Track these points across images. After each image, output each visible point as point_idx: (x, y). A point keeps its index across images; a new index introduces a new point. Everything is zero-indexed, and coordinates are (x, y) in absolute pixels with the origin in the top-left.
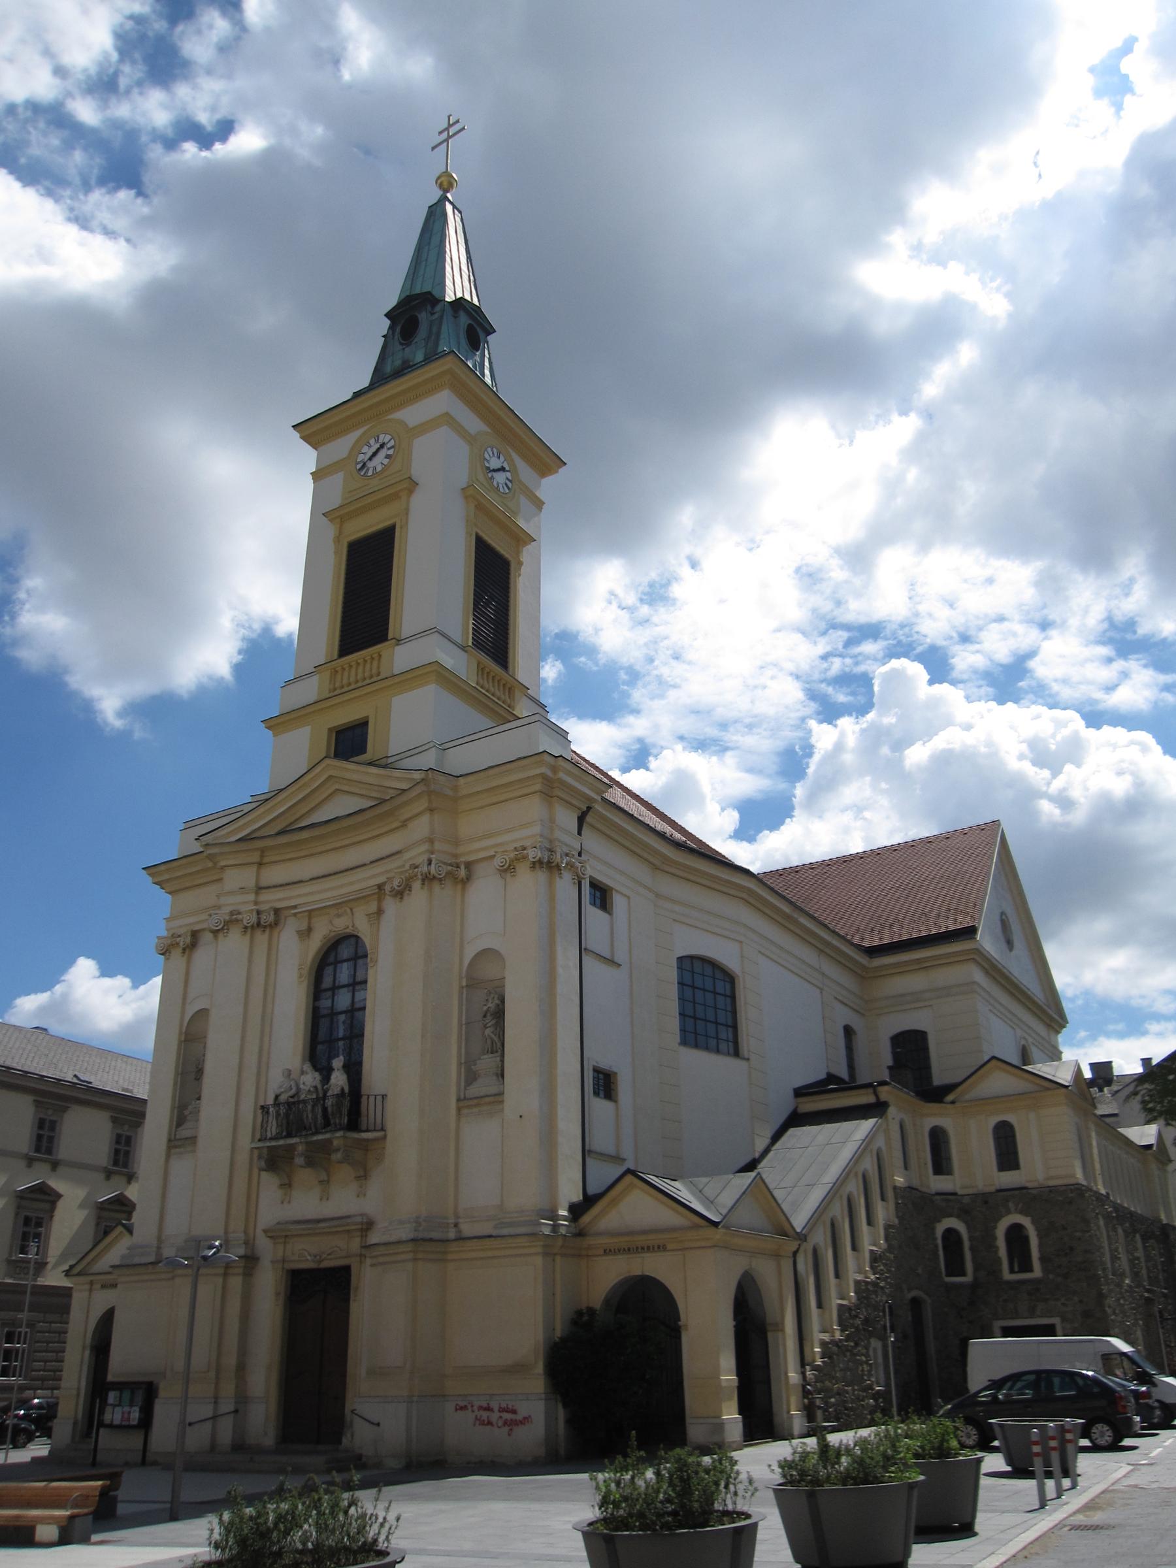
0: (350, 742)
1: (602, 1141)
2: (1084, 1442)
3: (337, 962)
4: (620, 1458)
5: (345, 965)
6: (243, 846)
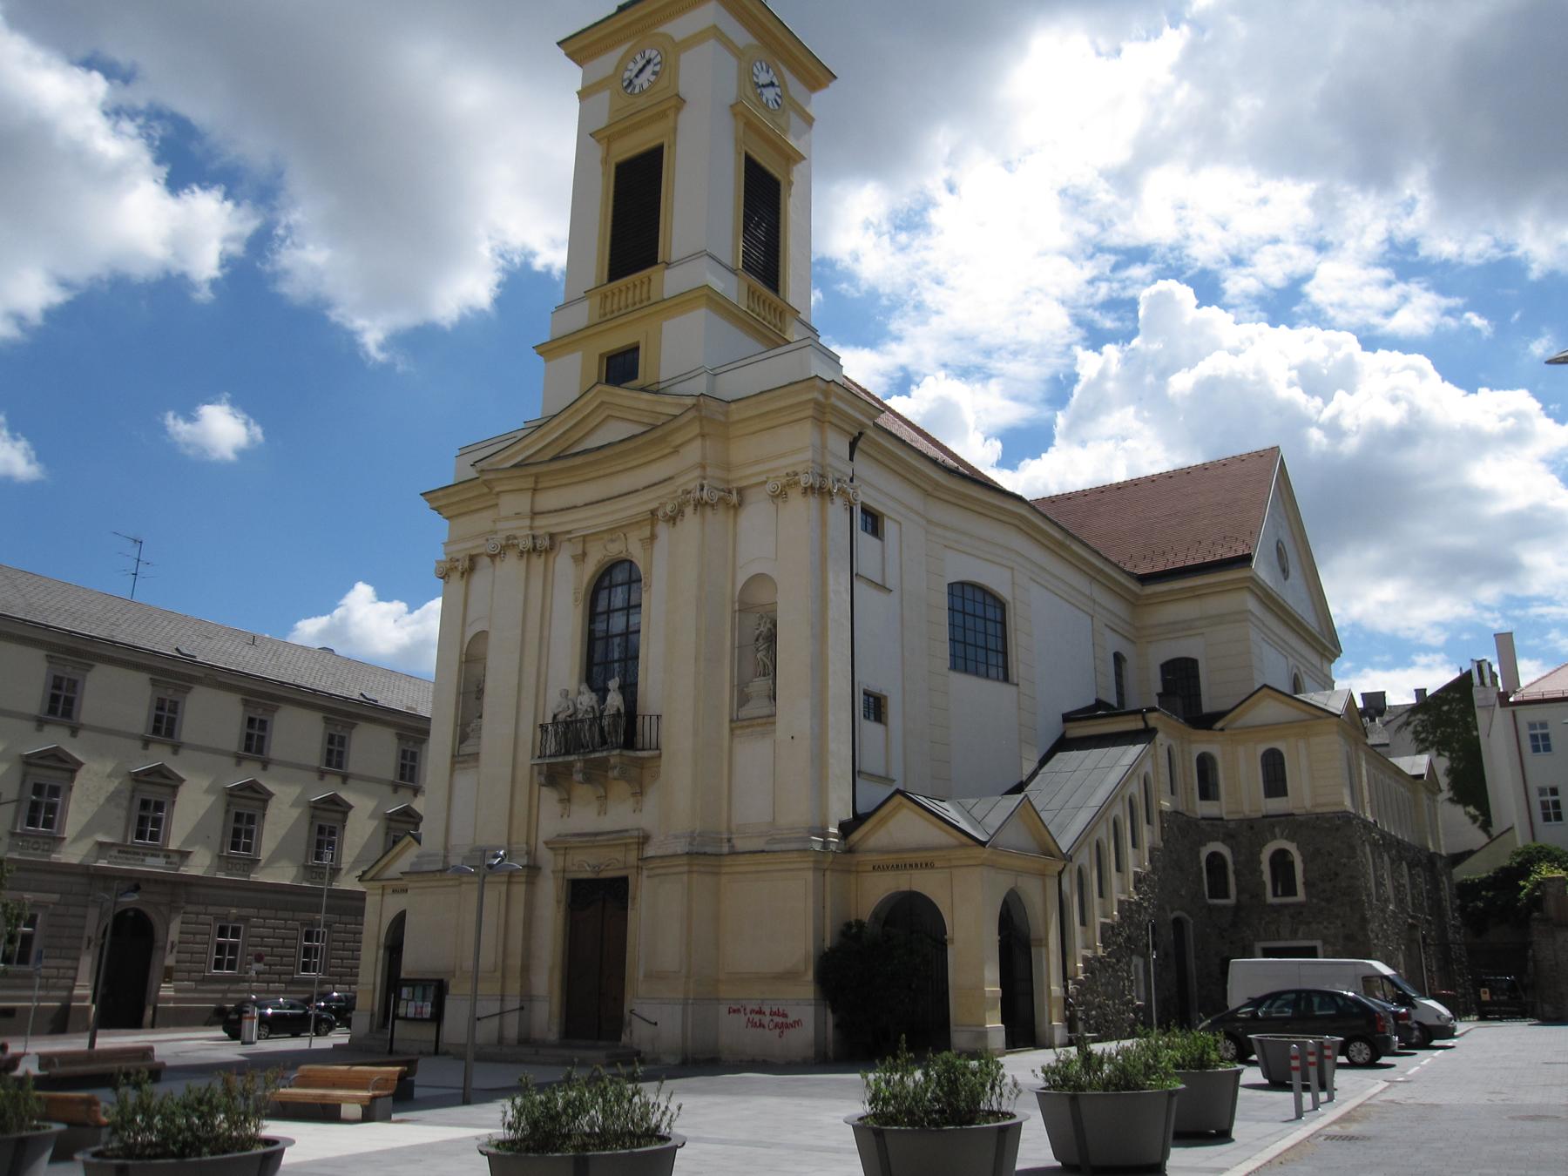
0: (621, 367)
1: (872, 761)
2: (1342, 1059)
3: (611, 587)
4: (890, 1059)
5: (619, 589)
6: (517, 472)
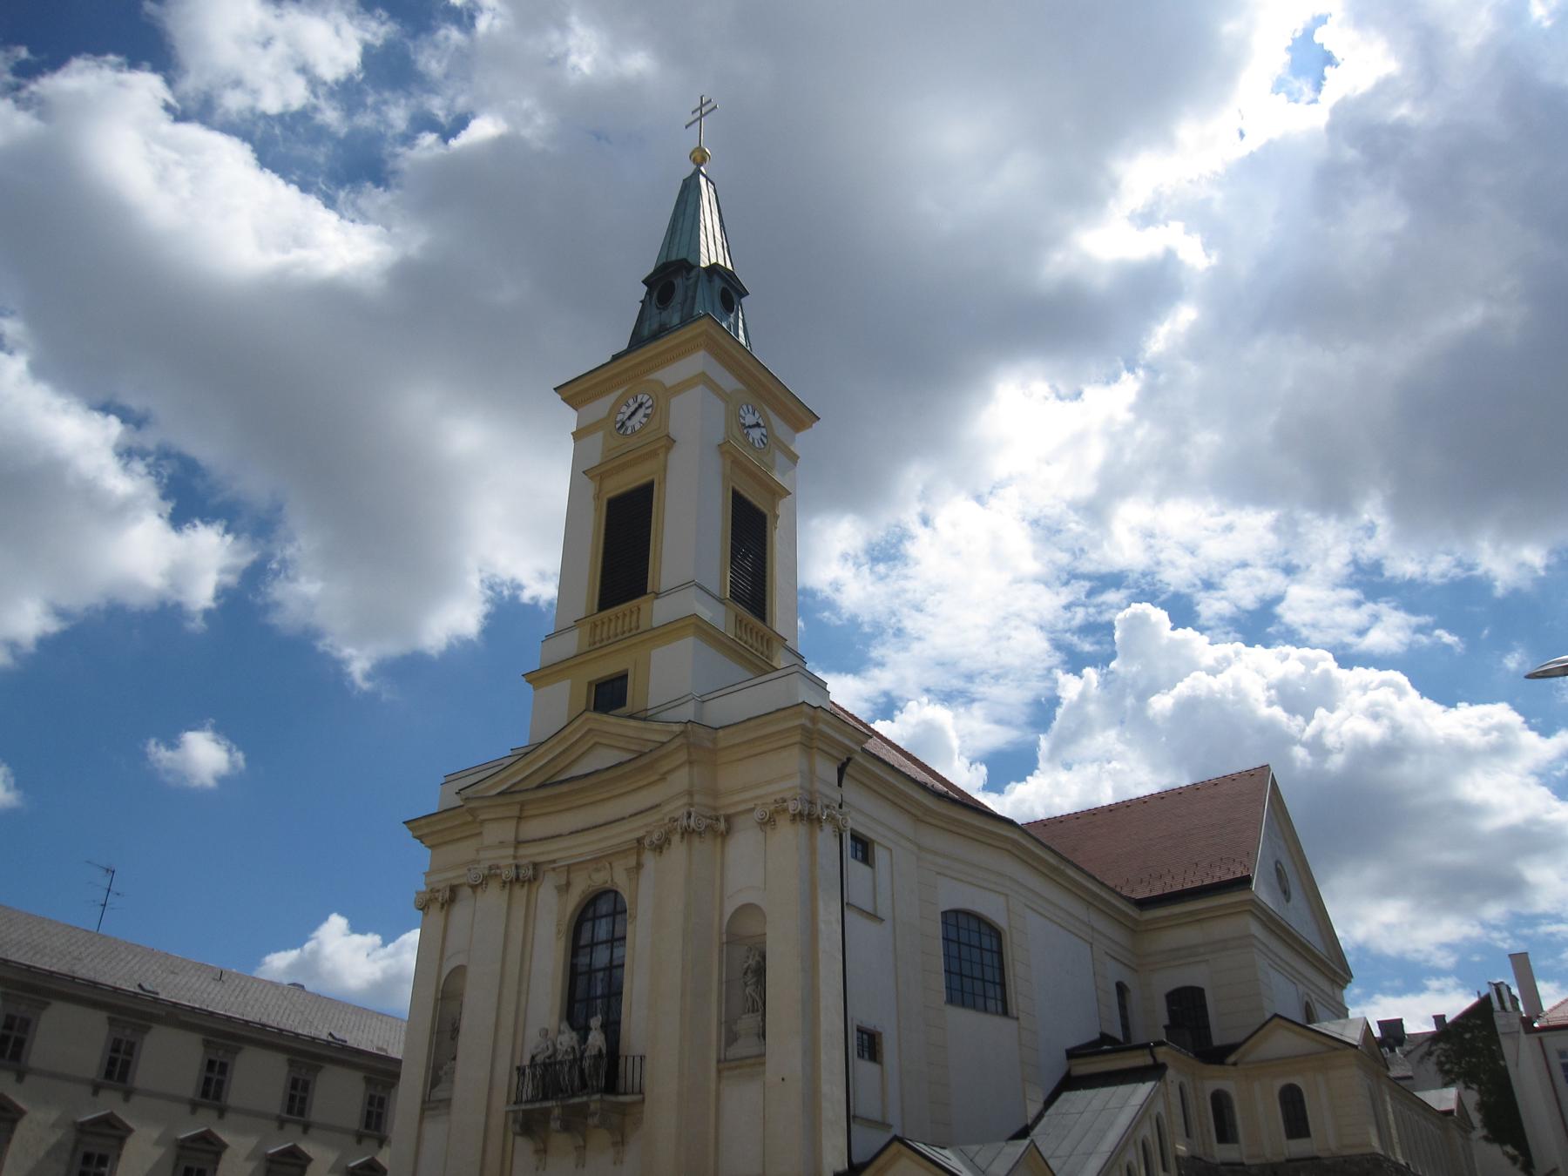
0: (609, 695)
1: (867, 1105)
3: (595, 919)
5: (604, 921)
